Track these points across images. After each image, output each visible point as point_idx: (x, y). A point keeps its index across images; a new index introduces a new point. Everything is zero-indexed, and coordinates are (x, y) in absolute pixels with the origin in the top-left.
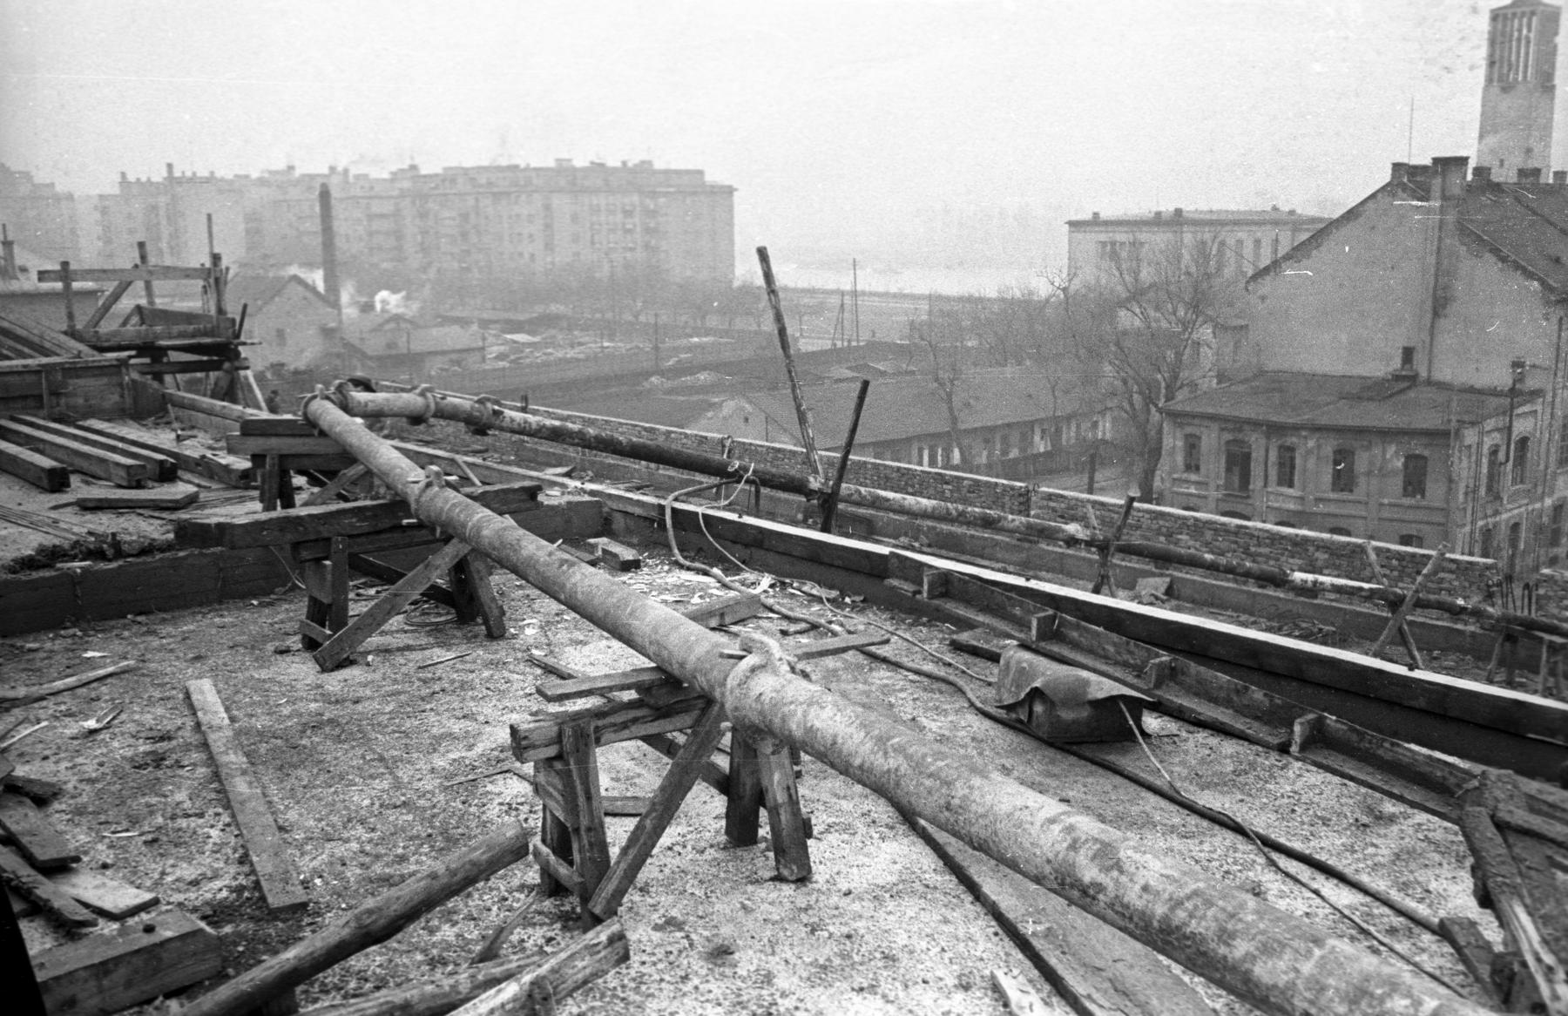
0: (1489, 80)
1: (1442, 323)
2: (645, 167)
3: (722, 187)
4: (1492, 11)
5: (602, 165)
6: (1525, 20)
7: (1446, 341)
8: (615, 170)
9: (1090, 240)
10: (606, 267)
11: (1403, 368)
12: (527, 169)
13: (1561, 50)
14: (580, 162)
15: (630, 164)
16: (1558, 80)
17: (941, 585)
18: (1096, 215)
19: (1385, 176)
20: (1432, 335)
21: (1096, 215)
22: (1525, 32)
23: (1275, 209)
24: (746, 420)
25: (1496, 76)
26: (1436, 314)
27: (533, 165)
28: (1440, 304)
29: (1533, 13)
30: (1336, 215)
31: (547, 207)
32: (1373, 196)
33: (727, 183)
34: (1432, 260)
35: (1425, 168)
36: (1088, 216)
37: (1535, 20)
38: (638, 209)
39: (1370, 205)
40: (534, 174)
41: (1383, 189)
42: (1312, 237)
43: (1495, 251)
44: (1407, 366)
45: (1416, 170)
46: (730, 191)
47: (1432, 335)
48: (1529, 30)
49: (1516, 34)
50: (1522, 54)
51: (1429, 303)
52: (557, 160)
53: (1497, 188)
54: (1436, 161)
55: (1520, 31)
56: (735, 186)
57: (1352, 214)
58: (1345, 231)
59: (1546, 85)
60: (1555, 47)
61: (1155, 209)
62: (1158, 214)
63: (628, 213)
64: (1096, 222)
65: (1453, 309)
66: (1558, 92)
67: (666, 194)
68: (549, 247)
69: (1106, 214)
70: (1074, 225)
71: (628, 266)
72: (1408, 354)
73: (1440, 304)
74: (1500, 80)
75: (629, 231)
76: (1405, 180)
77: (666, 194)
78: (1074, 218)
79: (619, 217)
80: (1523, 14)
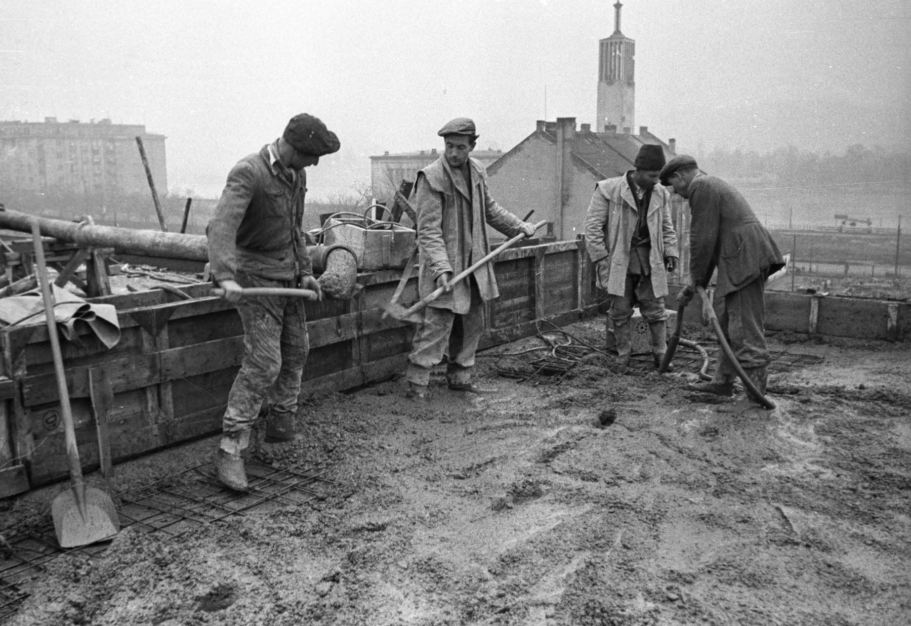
0: (601, 79)
1: (567, 210)
2: (106, 123)
3: (160, 136)
4: (600, 40)
5: (77, 122)
6: (617, 46)
7: (568, 218)
8: (85, 126)
9: (381, 166)
10: (82, 188)
11: (548, 235)
12: (26, 123)
13: (636, 62)
14: (62, 119)
15: (96, 122)
16: (636, 79)
17: (518, 500)
18: (387, 153)
19: (534, 128)
20: (562, 215)
21: (387, 153)
22: (618, 53)
23: (490, 149)
24: (684, 551)
25: (604, 76)
26: (563, 204)
27: (30, 121)
28: (565, 200)
29: (621, 43)
30: (506, 150)
31: (40, 148)
32: (527, 139)
33: (162, 133)
34: (560, 174)
35: (554, 124)
36: (382, 154)
37: (622, 46)
38: (102, 150)
39: (526, 143)
40: (31, 127)
41: (532, 135)
42: (497, 162)
43: (591, 170)
44: (550, 234)
45: (549, 125)
46: (162, 139)
47: (562, 215)
48: (620, 52)
49: (613, 54)
50: (617, 64)
51: (559, 199)
52: (46, 118)
53: (593, 136)
54: (559, 119)
55: (615, 52)
56: (166, 136)
57: (517, 149)
58: (515, 159)
59: (630, 83)
60: (633, 61)
61: (420, 149)
62: (422, 152)
63: (95, 152)
64: (386, 157)
65: (572, 201)
66: (637, 85)
67: (120, 140)
68: (42, 172)
69: (392, 153)
70: (375, 159)
71: (98, 187)
72: (550, 226)
73: (565, 200)
74: (606, 78)
75: (98, 163)
76: (544, 130)
77: (120, 140)
78: (373, 155)
79: (89, 155)
80: (616, 43)
